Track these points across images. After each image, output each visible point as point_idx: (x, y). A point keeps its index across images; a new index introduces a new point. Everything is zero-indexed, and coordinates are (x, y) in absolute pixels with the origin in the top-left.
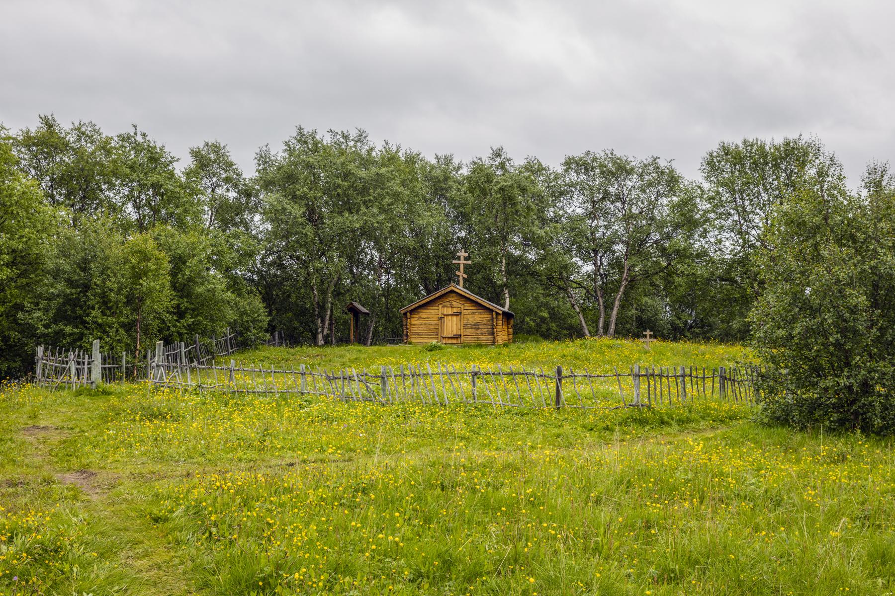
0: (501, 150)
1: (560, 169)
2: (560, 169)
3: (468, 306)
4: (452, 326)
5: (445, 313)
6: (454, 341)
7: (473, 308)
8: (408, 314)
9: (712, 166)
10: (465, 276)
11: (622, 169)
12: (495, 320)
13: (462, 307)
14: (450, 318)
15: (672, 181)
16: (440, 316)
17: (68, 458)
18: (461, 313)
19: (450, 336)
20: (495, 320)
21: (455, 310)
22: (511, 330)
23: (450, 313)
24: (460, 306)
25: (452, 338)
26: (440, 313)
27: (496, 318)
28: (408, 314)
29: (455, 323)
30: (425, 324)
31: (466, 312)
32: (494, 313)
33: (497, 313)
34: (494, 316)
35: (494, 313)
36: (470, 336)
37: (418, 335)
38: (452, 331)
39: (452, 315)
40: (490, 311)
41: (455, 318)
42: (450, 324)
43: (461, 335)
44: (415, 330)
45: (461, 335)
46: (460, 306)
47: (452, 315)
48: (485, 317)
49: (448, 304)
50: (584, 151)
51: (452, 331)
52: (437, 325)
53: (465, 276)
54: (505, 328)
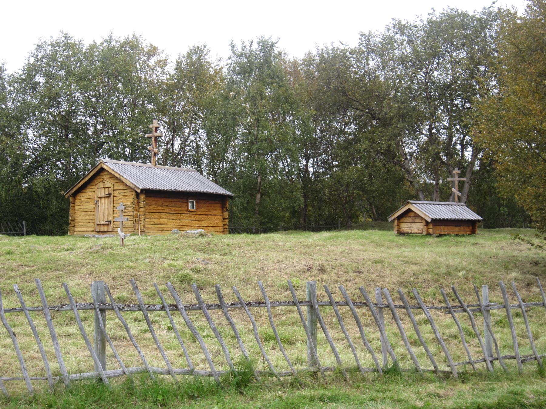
5: (100, 196)
14: (103, 200)
16: (97, 199)
19: (102, 222)
29: (106, 207)
38: (104, 217)
39: (105, 197)
41: (106, 200)
47: (105, 197)
49: (101, 185)
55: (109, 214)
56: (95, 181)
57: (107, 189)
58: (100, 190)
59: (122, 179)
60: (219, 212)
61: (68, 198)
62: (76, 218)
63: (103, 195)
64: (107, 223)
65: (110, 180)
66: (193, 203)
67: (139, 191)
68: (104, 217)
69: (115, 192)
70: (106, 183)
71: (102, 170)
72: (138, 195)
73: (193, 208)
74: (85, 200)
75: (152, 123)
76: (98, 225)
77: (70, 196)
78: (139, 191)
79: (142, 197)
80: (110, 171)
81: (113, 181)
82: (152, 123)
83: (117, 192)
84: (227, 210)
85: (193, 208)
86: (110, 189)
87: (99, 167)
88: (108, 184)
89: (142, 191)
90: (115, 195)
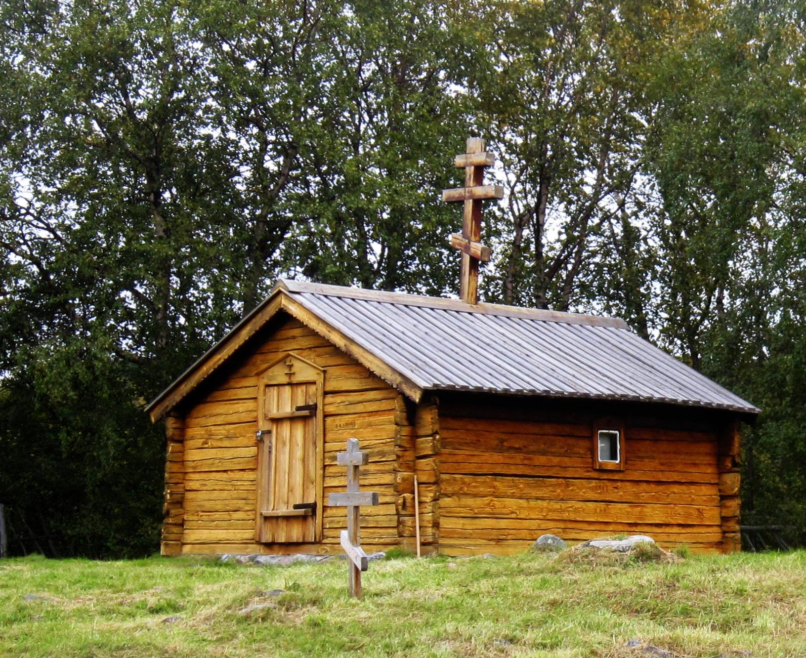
5: (274, 413)
14: (286, 428)
16: (263, 425)
19: (283, 510)
29: (299, 453)
31: (334, 404)
38: (291, 490)
39: (292, 419)
42: (285, 458)
47: (292, 419)
49: (279, 374)
55: (307, 480)
56: (260, 362)
57: (300, 391)
58: (274, 391)
59: (356, 351)
60: (708, 472)
61: (161, 420)
62: (189, 495)
63: (287, 409)
64: (301, 511)
65: (311, 358)
66: (612, 438)
67: (416, 397)
68: (291, 490)
69: (329, 399)
70: (297, 366)
71: (283, 319)
72: (412, 411)
73: (613, 456)
74: (222, 431)
75: (463, 150)
76: (267, 518)
77: (168, 414)
78: (416, 397)
79: (428, 419)
80: (313, 324)
81: (321, 361)
82: (463, 150)
83: (339, 399)
84: (735, 464)
85: (613, 456)
86: (312, 389)
87: (271, 310)
88: (304, 372)
89: (427, 394)
90: (330, 409)
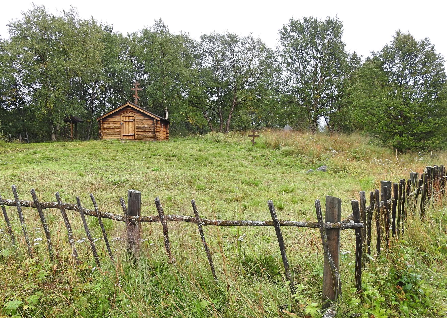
0: (160, 22)
1: (199, 41)
2: (199, 41)
3: (139, 116)
4: (129, 128)
5: (125, 120)
6: (130, 138)
7: (142, 117)
8: (101, 121)
9: (285, 35)
10: (139, 98)
11: (233, 40)
12: (155, 124)
13: (135, 116)
14: (127, 123)
15: (262, 48)
17: (239, 168)
18: (134, 120)
19: (127, 135)
20: (155, 124)
21: (131, 118)
22: (168, 132)
23: (128, 120)
24: (133, 115)
25: (128, 136)
26: (121, 121)
27: (157, 123)
28: (101, 121)
29: (131, 126)
30: (112, 127)
31: (138, 120)
32: (155, 120)
33: (157, 120)
34: (155, 122)
35: (155, 120)
36: (140, 133)
37: (108, 134)
38: (129, 132)
40: (153, 119)
41: (130, 123)
43: (134, 134)
44: (106, 131)
45: (134, 134)
46: (133, 115)
48: (150, 122)
49: (126, 115)
50: (212, 31)
51: (129, 132)
52: (119, 128)
53: (139, 98)
54: (164, 130)
